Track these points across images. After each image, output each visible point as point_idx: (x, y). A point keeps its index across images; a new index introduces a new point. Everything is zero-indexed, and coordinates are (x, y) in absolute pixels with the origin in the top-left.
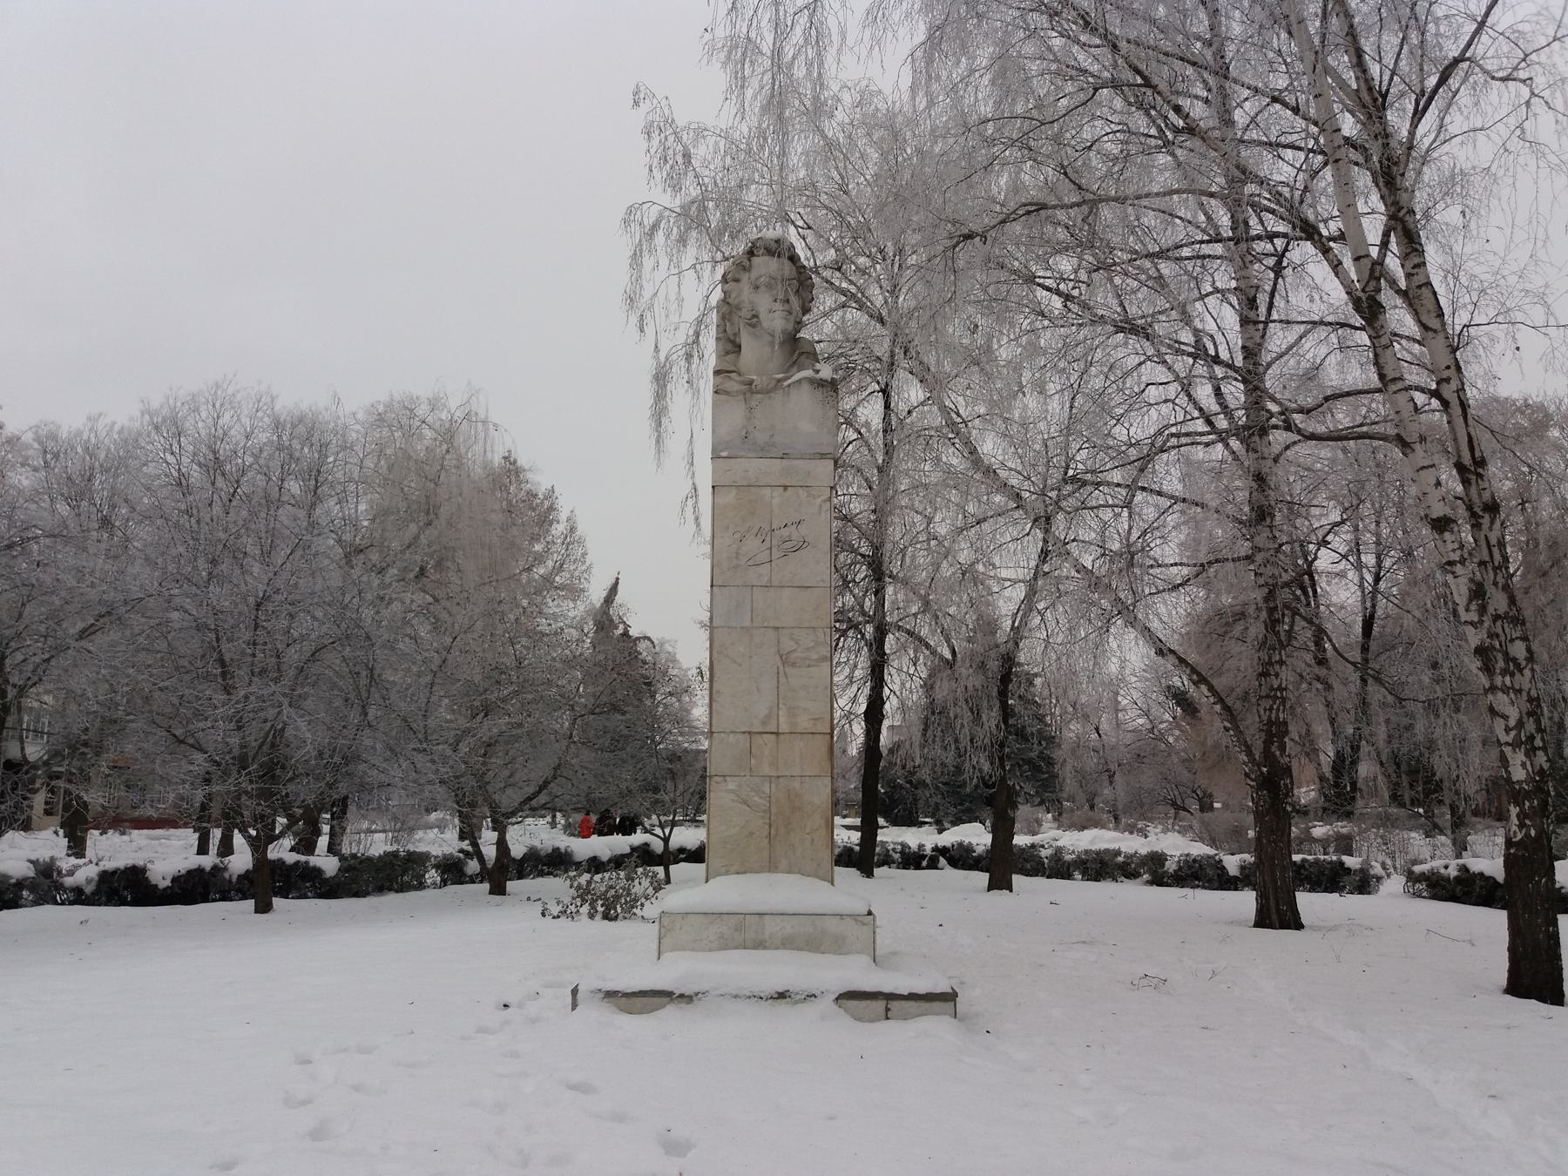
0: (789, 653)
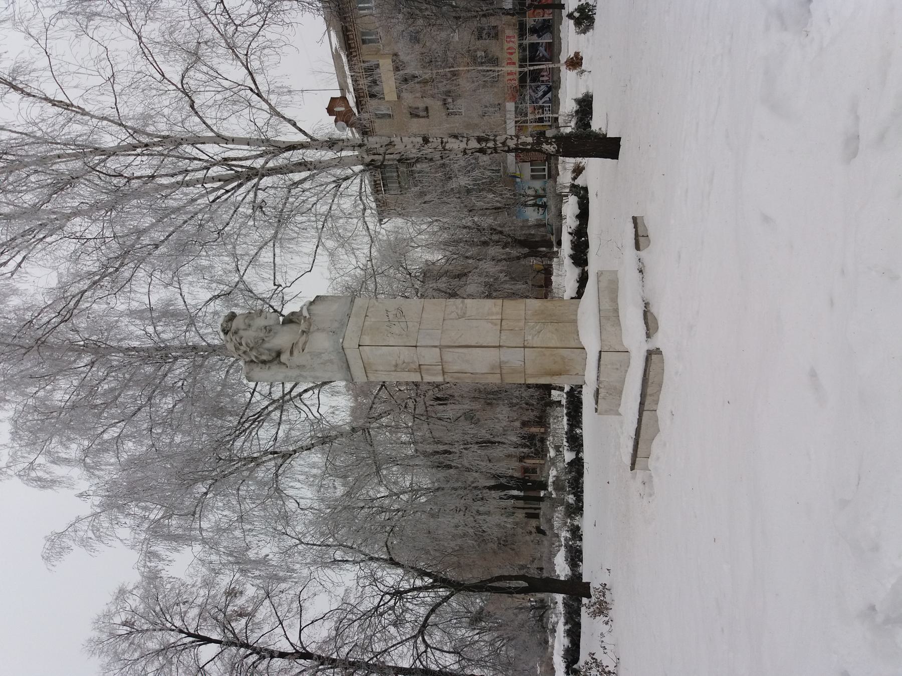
0: (458, 315)
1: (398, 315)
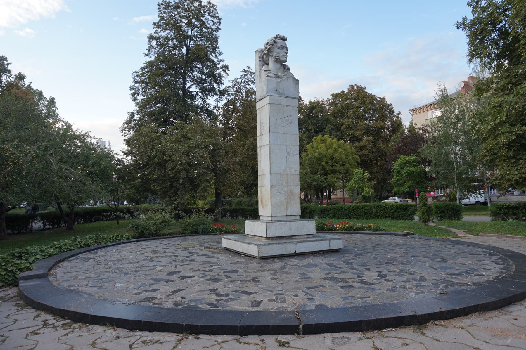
1: (288, 122)
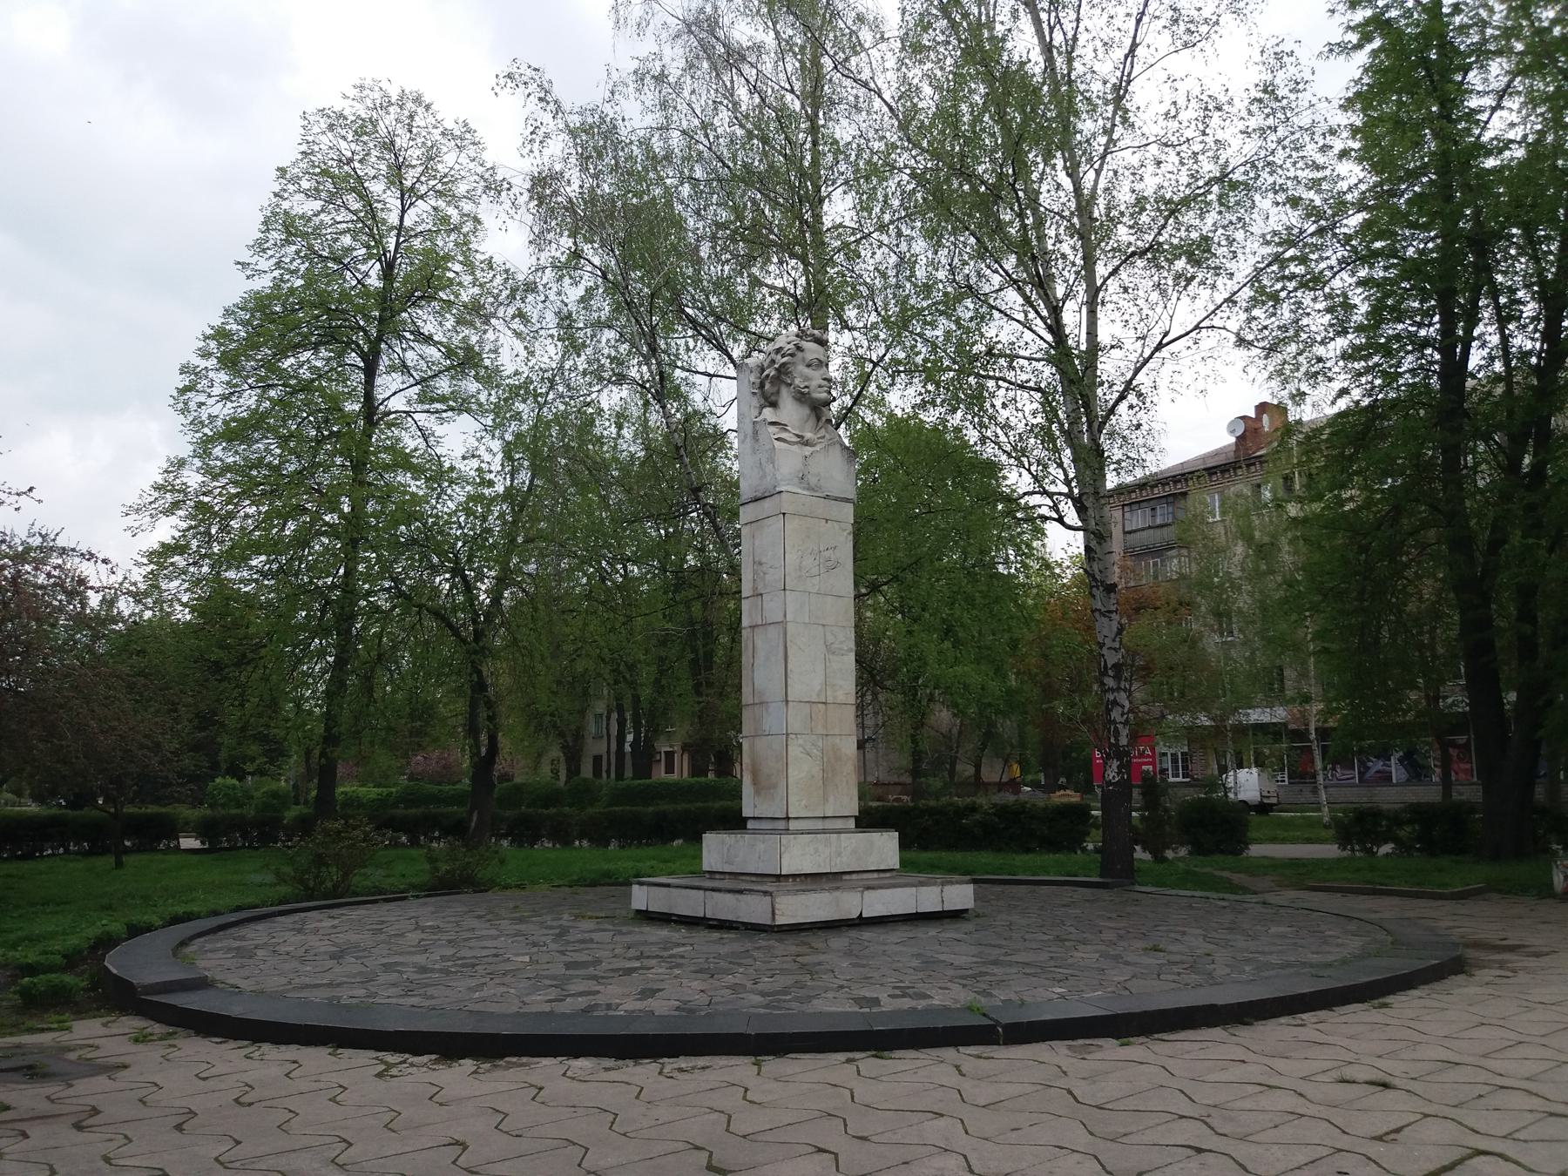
1: (829, 564)
